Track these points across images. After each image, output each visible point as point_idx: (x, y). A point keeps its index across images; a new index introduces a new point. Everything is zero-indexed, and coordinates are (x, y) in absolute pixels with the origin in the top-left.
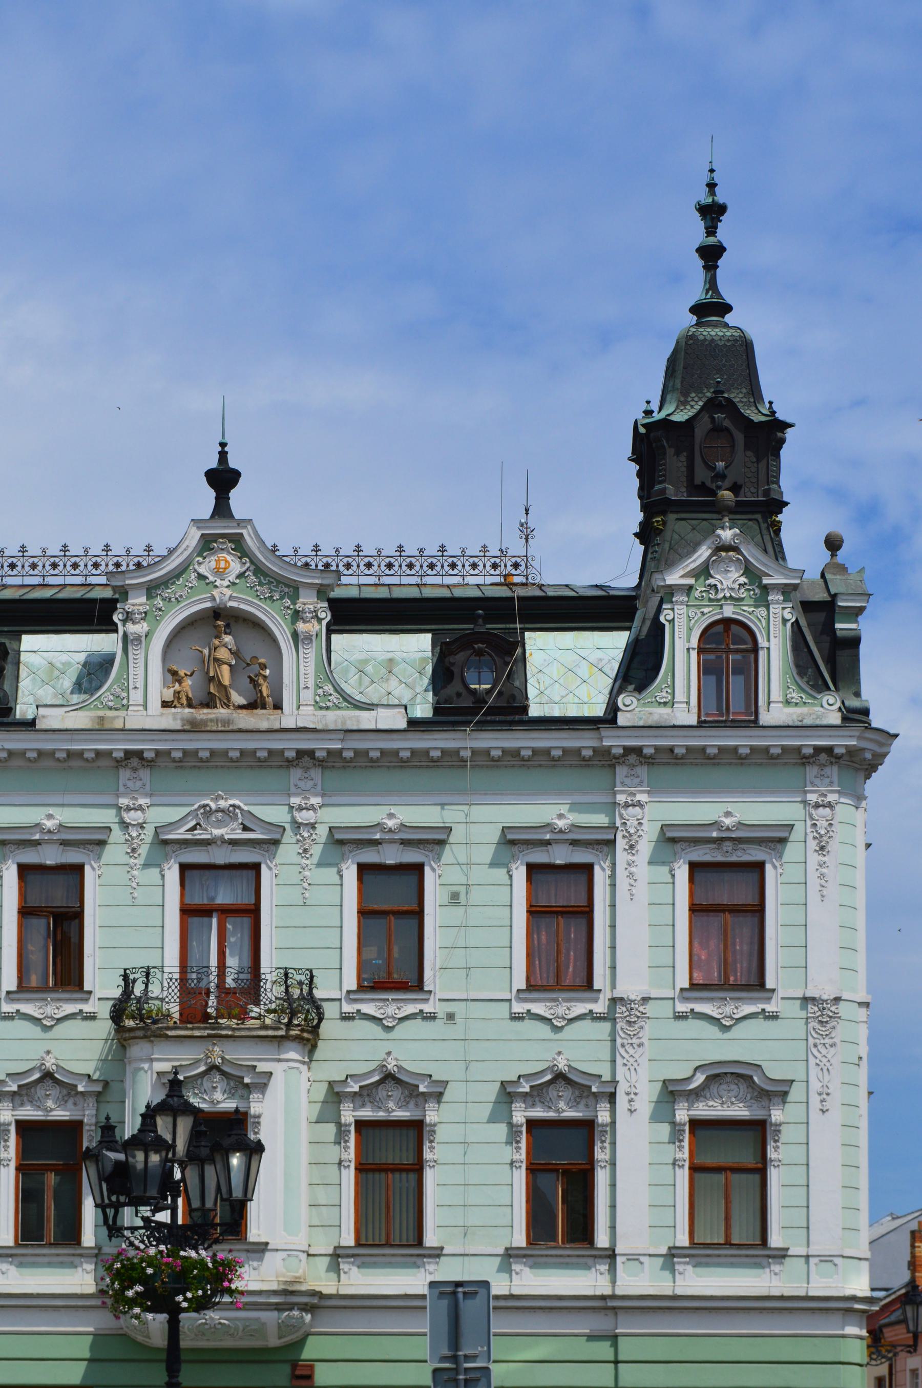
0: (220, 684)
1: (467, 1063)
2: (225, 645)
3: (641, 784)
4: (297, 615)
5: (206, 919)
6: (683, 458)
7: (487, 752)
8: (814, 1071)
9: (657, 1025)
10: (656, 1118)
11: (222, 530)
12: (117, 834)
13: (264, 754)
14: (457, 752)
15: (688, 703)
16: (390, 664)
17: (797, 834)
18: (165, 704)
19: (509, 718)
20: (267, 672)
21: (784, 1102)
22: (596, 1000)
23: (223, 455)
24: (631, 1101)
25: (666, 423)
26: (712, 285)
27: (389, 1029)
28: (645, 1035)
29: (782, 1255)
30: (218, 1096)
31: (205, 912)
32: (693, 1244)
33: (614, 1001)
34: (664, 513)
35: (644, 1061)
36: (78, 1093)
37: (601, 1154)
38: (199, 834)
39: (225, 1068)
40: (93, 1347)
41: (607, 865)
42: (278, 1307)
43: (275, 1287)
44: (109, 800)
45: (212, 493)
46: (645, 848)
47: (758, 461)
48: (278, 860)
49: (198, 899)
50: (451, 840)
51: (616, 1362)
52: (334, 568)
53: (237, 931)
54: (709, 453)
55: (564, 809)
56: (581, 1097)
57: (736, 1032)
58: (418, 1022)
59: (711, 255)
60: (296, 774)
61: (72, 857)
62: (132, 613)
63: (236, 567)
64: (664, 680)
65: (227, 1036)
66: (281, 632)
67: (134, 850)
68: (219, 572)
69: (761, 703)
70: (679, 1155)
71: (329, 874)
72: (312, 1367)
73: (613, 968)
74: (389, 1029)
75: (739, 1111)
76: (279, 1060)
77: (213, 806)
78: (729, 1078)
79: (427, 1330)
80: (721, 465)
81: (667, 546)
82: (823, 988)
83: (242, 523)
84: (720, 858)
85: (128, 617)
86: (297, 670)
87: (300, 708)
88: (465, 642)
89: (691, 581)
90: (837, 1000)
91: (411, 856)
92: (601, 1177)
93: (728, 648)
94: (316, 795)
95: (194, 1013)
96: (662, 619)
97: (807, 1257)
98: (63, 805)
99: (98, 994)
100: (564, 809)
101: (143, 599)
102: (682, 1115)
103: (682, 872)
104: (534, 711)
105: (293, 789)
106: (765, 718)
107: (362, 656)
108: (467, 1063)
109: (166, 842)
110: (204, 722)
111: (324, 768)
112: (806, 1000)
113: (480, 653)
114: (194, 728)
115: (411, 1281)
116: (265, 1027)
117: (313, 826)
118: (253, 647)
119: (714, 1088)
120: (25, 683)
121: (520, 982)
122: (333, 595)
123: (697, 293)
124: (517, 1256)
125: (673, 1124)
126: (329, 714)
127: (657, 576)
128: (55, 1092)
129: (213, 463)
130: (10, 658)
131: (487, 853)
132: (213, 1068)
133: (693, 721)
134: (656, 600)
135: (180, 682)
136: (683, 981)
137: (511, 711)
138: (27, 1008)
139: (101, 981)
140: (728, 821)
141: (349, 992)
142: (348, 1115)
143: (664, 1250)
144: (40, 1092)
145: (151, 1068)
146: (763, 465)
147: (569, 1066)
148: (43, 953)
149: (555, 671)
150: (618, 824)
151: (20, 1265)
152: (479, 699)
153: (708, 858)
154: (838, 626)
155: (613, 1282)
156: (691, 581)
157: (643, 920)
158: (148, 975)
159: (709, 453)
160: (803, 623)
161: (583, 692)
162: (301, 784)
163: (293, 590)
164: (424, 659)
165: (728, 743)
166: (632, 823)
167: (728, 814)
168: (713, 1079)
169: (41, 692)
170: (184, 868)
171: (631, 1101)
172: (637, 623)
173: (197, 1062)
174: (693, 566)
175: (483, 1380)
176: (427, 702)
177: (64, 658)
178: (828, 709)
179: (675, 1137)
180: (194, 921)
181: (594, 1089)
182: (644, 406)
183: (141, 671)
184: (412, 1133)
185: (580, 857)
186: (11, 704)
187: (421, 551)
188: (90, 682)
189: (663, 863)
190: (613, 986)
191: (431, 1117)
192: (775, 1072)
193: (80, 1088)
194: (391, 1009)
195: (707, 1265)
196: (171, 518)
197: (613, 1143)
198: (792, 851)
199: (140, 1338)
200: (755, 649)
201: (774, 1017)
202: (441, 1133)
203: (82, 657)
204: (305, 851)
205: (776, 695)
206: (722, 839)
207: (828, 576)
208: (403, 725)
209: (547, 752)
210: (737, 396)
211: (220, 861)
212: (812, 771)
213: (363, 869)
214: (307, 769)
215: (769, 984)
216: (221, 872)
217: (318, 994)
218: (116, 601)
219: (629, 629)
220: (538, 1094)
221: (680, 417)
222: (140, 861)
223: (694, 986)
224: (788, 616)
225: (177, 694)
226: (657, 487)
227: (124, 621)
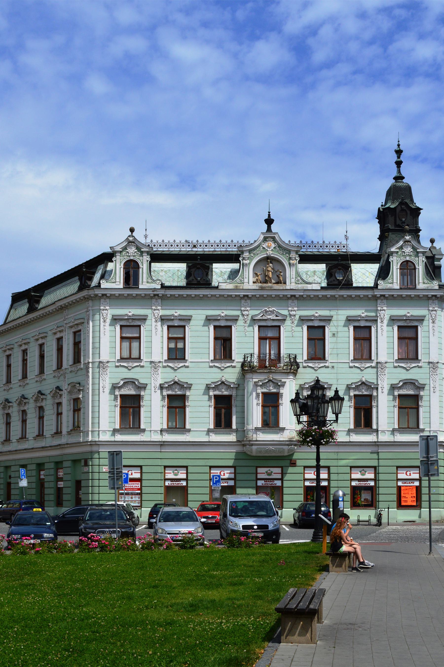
0: (269, 277)
1: (338, 380)
2: (270, 267)
3: (384, 305)
4: (290, 259)
5: (265, 341)
6: (393, 217)
7: (343, 296)
8: (431, 382)
9: (111, 369)
10: (389, 394)
11: (270, 235)
12: (241, 318)
13: (202, 296)
14: (334, 296)
15: (120, 282)
16: (315, 272)
17: (427, 318)
18: (254, 282)
19: (348, 287)
20: (282, 274)
21: (190, 390)
22: (372, 363)
23: (269, 215)
24: (382, 390)
25: (389, 208)
26: (399, 172)
27: (316, 370)
28: (386, 372)
29: (189, 431)
30: (271, 388)
31: (265, 339)
32: (399, 428)
33: (377, 363)
34: (388, 232)
35: (386, 379)
36: (231, 387)
37: (374, 404)
38: (264, 318)
39: (273, 381)
40: (235, 456)
41: (375, 326)
42: (288, 445)
43: (287, 439)
44: (239, 308)
45: (266, 226)
46: (386, 322)
47: (413, 219)
48: (285, 325)
49: (263, 335)
50: (333, 319)
51: (378, 459)
52: (150, 246)
53: (274, 344)
54: (399, 217)
55: (363, 311)
56: (368, 388)
58: (139, 368)
59: (399, 164)
60: (290, 301)
61: (229, 324)
62: (245, 258)
63: (273, 245)
64: (391, 277)
65: (273, 372)
66: (286, 263)
67: (246, 322)
68: (269, 247)
69: (417, 283)
70: (395, 404)
71: (299, 329)
72: (296, 461)
73: (377, 354)
74: (316, 370)
75: (411, 392)
76: (288, 378)
77: (268, 310)
78: (409, 383)
79: (419, 451)
80: (404, 219)
81: (389, 241)
82: (433, 359)
83: (274, 233)
84: (406, 325)
85: (244, 259)
86: (290, 273)
87: (291, 284)
88: (336, 266)
89: (398, 250)
90: (438, 363)
91: (322, 324)
92: (374, 410)
93: (408, 268)
94: (296, 307)
95: (262, 365)
96: (390, 260)
97: (151, 431)
98: (226, 310)
99: (236, 360)
100: (363, 311)
101: (248, 254)
102: (396, 393)
103: (396, 328)
104: (354, 285)
105: (289, 305)
106: (418, 287)
107: (307, 270)
108: (338, 380)
109: (254, 320)
110: (265, 287)
111: (298, 300)
112: (429, 363)
113: (340, 269)
114: (262, 289)
115: (415, 438)
116: (284, 370)
117: (295, 315)
118: (278, 267)
119: (405, 386)
120: (214, 277)
121: (212, 358)
122: (299, 253)
123: (395, 173)
124: (351, 431)
125: (394, 396)
126: (299, 285)
127: (389, 249)
128: (225, 387)
129: (267, 217)
130: (210, 270)
131: (342, 323)
132: (270, 380)
133: (398, 288)
134: (387, 255)
135: (258, 276)
136: (396, 358)
137: (348, 285)
138: (217, 364)
139: (237, 356)
140: (408, 315)
141: (305, 360)
142: (211, 393)
143: (391, 430)
144: (220, 387)
145: (252, 381)
146: (415, 220)
147: (178, 380)
148: (220, 349)
149: (359, 274)
150: (378, 315)
151: (215, 434)
152: (340, 282)
153: (403, 325)
154: (435, 263)
155: (378, 438)
156: (398, 250)
157: (385, 341)
158: (251, 355)
159: (399, 217)
160: (427, 262)
161: (368, 280)
162: (292, 304)
163: (289, 252)
164: (324, 271)
165: (408, 294)
166: (382, 315)
167: (408, 313)
168: (404, 384)
169: (219, 279)
170: (259, 327)
171: (382, 390)
172: (381, 262)
173: (265, 379)
174: (398, 246)
175: (436, 464)
176: (325, 282)
177: (225, 270)
178: (435, 285)
179: (394, 399)
180: (262, 341)
181: (372, 386)
182: (381, 204)
183: (247, 273)
184: (369, 398)
185: (368, 324)
186: (211, 282)
187: (318, 242)
188: (232, 276)
189: (390, 326)
190: (377, 359)
191: (188, 393)
192: (421, 382)
193: (232, 386)
194: (317, 365)
195: (403, 433)
196: (254, 233)
197: (377, 401)
198: (425, 323)
199: (249, 453)
200: (415, 269)
201: (143, 367)
202: (190, 398)
203: (230, 270)
204: (293, 322)
205: (145, 280)
206: (407, 320)
207: (432, 250)
208: (319, 288)
209: (359, 296)
210: (408, 201)
211: (269, 325)
212: (431, 301)
213: (309, 327)
214: (157, 299)
215: (419, 358)
216: (269, 328)
217: (298, 361)
218: (240, 254)
219: (379, 263)
220: (216, 388)
221: (392, 206)
223: (399, 359)
224: (424, 260)
225: (257, 279)
226: (386, 225)
227: (243, 260)
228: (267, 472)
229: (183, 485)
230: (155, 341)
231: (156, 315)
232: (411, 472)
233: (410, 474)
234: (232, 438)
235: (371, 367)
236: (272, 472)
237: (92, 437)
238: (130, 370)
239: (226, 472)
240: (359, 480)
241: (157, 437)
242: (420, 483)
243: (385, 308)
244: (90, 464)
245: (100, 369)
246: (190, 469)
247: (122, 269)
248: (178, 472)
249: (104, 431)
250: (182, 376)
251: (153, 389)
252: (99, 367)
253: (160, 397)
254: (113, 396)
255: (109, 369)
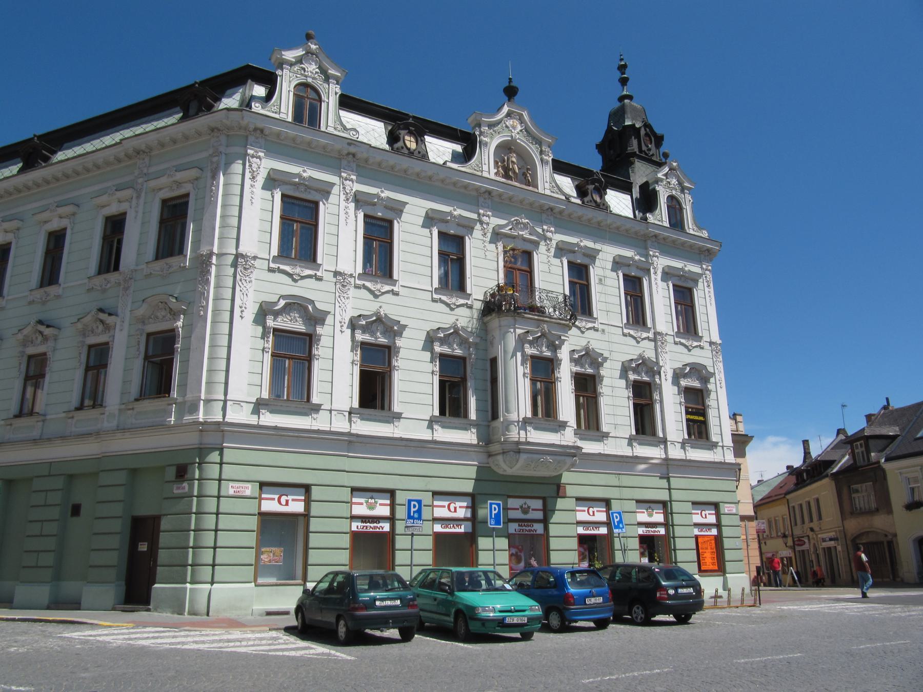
8: (337, 309)
9: (259, 272)
17: (335, 190)
24: (242, 312)
28: (253, 276)
29: (398, 416)
35: (251, 291)
37: (656, 397)
57: (300, 283)
58: (313, 280)
68: (514, 128)
112: (336, 274)
117: (488, 224)
125: (264, 327)
131: (609, 265)
155: (224, 416)
166: (255, 166)
171: (242, 312)
179: (264, 336)
198: (333, 198)
200: (320, 100)
201: (319, 279)
202: (402, 353)
222: (488, 240)
228: (521, 507)
229: (385, 530)
230: (341, 235)
231: (348, 189)
232: (290, 498)
233: (287, 501)
234: (469, 437)
235: (648, 338)
236: (529, 507)
237: (206, 413)
238: (295, 281)
239: (458, 504)
240: (364, 519)
241: (341, 425)
242: (720, 531)
243: (262, 154)
244: (197, 476)
245: (239, 270)
246: (316, 493)
247: (292, 94)
248: (376, 503)
249: (238, 402)
250: (390, 307)
251: (338, 325)
252: (235, 265)
253: (349, 344)
254: (260, 329)
255: (256, 272)
